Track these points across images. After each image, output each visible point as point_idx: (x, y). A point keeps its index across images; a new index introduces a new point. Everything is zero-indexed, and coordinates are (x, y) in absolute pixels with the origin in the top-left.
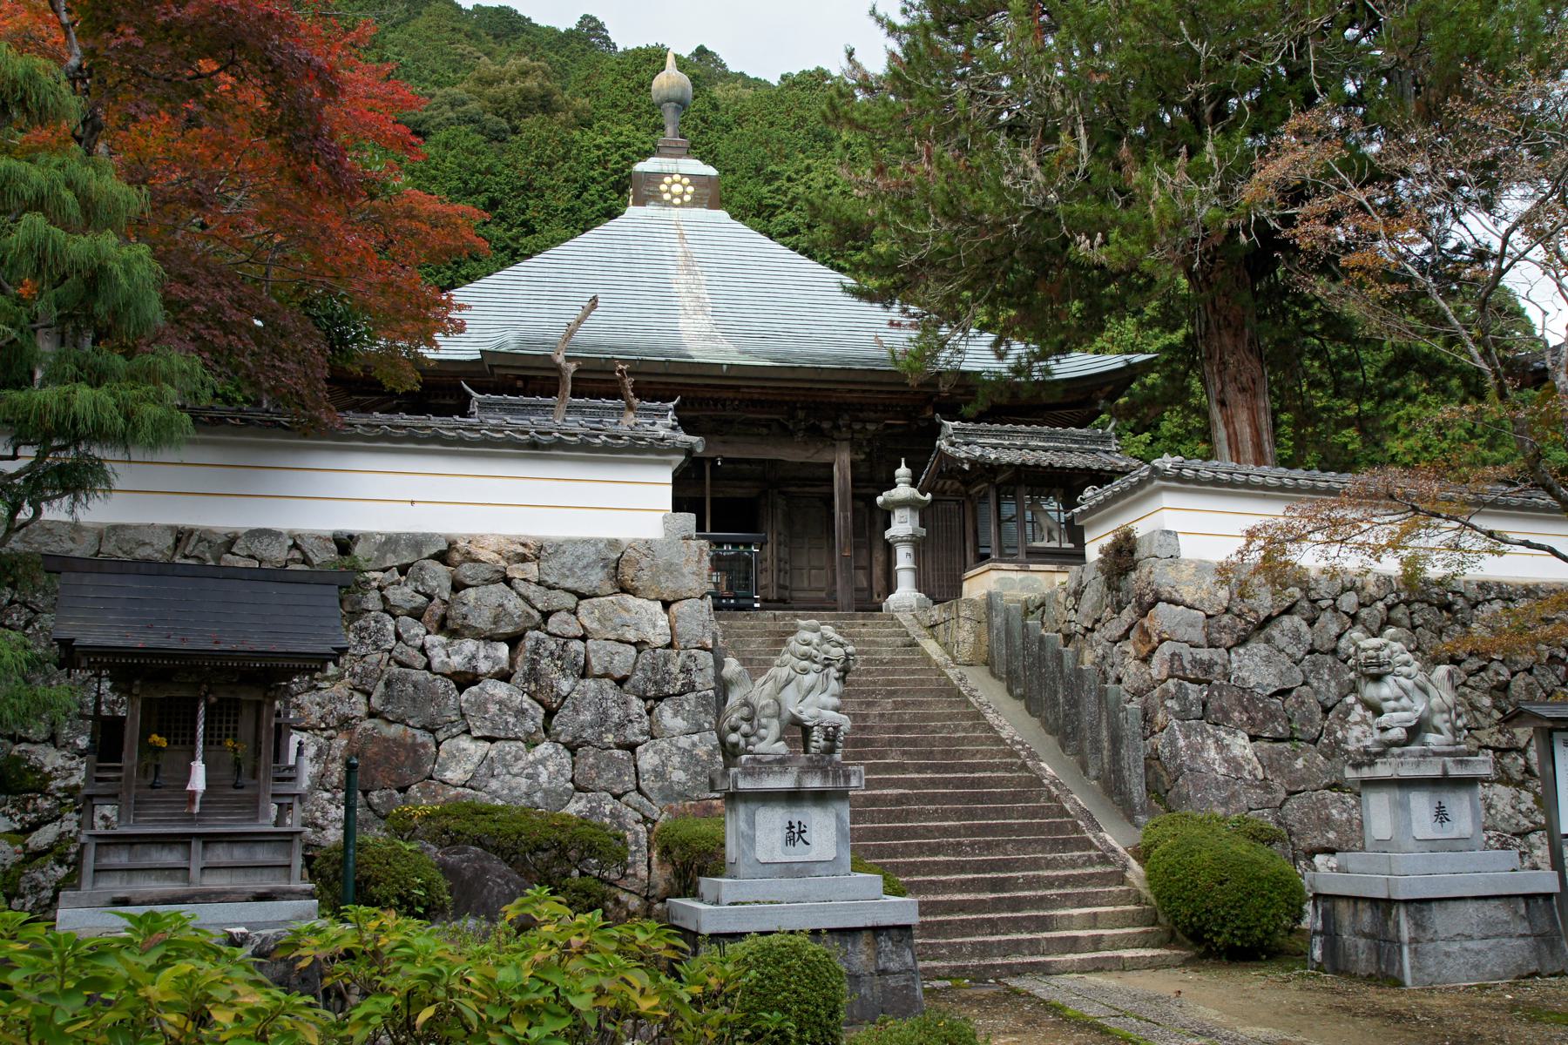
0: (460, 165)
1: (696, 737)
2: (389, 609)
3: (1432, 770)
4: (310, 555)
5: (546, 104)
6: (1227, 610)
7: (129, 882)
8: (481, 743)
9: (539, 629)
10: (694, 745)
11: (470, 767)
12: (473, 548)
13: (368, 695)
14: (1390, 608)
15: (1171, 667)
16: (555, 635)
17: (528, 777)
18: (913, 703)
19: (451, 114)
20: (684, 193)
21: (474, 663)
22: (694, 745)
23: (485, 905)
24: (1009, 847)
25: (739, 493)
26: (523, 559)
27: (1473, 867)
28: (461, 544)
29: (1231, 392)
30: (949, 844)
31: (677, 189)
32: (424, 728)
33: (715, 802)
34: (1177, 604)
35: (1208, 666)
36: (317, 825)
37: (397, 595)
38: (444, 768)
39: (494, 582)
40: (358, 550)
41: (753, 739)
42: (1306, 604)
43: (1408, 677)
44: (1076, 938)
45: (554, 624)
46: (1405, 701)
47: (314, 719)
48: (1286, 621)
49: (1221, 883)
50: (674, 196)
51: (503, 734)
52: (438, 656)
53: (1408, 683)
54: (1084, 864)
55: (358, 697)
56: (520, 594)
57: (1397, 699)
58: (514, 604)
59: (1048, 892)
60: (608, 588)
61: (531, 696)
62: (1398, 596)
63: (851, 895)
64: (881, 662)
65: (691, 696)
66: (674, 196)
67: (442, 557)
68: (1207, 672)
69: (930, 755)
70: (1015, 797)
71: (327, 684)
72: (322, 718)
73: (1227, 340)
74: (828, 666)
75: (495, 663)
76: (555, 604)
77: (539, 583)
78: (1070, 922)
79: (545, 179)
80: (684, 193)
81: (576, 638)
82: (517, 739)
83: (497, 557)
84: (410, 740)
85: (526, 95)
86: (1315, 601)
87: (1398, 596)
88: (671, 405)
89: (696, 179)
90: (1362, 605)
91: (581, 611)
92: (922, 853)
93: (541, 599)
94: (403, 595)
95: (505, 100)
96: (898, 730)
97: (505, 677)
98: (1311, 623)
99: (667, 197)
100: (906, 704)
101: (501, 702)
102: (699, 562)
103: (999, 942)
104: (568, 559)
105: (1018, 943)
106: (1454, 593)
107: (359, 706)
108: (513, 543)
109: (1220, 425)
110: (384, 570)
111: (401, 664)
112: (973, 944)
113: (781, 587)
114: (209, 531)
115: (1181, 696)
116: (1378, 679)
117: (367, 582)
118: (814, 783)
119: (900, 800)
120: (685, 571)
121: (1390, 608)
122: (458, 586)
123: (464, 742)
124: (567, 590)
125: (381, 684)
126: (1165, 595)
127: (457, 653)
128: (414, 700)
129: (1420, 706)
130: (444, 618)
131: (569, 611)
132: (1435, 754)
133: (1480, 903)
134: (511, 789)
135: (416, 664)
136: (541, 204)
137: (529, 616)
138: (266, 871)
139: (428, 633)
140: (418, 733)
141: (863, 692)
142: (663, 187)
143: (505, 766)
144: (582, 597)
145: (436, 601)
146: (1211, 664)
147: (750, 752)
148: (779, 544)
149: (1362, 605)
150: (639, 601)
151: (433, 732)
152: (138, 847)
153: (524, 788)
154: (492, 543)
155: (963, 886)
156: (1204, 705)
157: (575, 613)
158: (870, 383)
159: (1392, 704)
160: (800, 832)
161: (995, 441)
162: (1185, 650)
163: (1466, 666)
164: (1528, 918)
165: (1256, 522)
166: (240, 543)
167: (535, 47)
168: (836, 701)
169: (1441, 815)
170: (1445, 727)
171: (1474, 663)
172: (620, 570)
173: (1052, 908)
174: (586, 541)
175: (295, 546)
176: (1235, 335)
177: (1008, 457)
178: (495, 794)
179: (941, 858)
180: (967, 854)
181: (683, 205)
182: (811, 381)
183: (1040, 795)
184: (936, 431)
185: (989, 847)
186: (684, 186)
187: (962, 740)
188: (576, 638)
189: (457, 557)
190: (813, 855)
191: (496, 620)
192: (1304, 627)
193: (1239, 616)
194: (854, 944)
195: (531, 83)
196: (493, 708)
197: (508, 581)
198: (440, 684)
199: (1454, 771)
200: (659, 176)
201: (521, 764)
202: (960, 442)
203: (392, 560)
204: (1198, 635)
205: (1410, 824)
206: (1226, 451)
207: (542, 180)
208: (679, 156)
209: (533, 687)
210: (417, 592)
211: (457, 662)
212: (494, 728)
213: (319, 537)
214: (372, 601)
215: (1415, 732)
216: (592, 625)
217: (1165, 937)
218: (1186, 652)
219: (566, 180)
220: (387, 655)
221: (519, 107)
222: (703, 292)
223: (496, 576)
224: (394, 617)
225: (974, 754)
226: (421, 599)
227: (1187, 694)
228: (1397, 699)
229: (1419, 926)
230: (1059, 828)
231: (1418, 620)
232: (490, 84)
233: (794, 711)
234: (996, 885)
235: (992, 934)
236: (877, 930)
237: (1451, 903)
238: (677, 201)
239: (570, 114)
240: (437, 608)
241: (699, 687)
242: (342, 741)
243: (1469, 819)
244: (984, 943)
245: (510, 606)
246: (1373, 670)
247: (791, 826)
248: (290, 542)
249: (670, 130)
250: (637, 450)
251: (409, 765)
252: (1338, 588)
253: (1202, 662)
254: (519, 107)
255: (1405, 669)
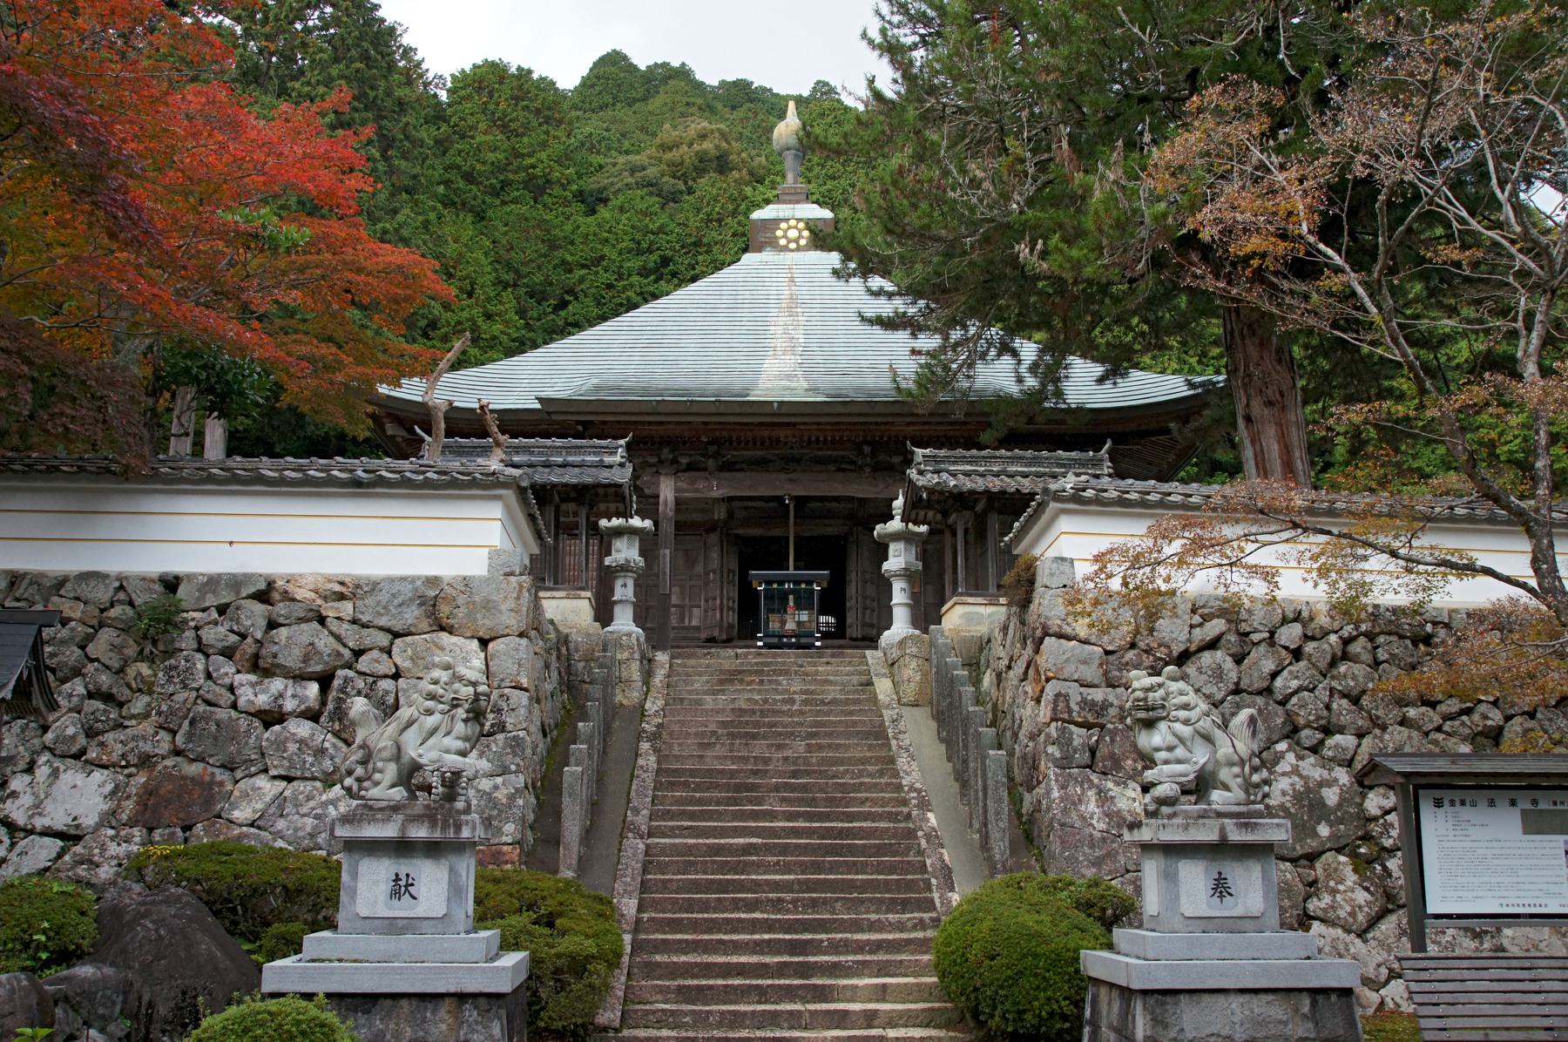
0: (633, 227)
1: (499, 780)
2: (201, 648)
3: (1206, 833)
4: (134, 596)
5: (722, 164)
6: (1133, 646)
8: (277, 783)
9: (350, 668)
10: (496, 787)
11: (260, 806)
12: (290, 588)
14: (1346, 642)
15: (1054, 709)
16: (364, 674)
17: (317, 817)
18: (830, 746)
19: (630, 180)
20: (800, 237)
21: (280, 701)
22: (496, 787)
23: (123, 951)
24: (838, 905)
25: (829, 531)
26: (341, 597)
27: (1217, 954)
28: (280, 583)
29: (1257, 408)
30: (769, 900)
31: (793, 234)
32: (223, 766)
33: (505, 848)
34: (1068, 638)
35: (1101, 708)
37: (209, 635)
38: (234, 807)
39: (308, 621)
40: (182, 591)
41: (366, 784)
42: (1233, 638)
43: (1186, 722)
44: (846, 1013)
45: (364, 664)
46: (1180, 752)
47: (115, 757)
48: (1207, 658)
49: (992, 958)
50: (790, 241)
51: (299, 774)
52: (246, 696)
53: (1185, 731)
54: (914, 928)
55: (162, 733)
56: (332, 633)
57: (1170, 749)
58: (325, 642)
59: (842, 958)
60: (424, 625)
61: (336, 734)
62: (1357, 628)
63: (448, 957)
64: (823, 702)
65: (500, 737)
66: (790, 241)
67: (263, 596)
68: (1099, 715)
69: (812, 802)
70: (880, 850)
71: (134, 722)
72: (123, 756)
73: (1253, 351)
74: (456, 706)
75: (302, 702)
76: (367, 642)
77: (354, 622)
78: (853, 994)
79: (714, 234)
80: (800, 237)
81: (386, 676)
82: (314, 779)
83: (313, 595)
84: (207, 778)
85: (702, 158)
86: (1247, 634)
87: (1357, 628)
88: (622, 442)
89: (812, 226)
90: (1307, 638)
91: (395, 650)
92: (737, 909)
93: (353, 637)
94: (217, 634)
95: (682, 163)
96: (794, 775)
97: (313, 716)
98: (1239, 660)
99: (783, 242)
100: (820, 747)
101: (302, 742)
102: (518, 598)
103: (753, 1012)
104: (383, 597)
105: (776, 1014)
106: (1435, 624)
107: (164, 743)
108: (330, 581)
109: (1247, 443)
110: (204, 610)
111: (209, 703)
112: (722, 1013)
113: (864, 625)
114: (43, 575)
115: (1064, 741)
116: (1149, 724)
117: (185, 621)
118: (420, 832)
119: (748, 849)
120: (503, 608)
121: (1346, 642)
122: (272, 625)
123: (262, 782)
124: (381, 629)
125: (187, 722)
126: (1055, 629)
127: (263, 691)
128: (215, 738)
129: (1201, 756)
130: (256, 656)
131: (382, 650)
132: (1219, 815)
133: (1247, 997)
134: (296, 830)
135: (222, 703)
136: (709, 258)
137: (339, 654)
139: (239, 672)
140: (217, 771)
141: (780, 734)
142: (779, 233)
143: (296, 806)
144: (397, 635)
145: (249, 640)
146: (1106, 705)
147: (362, 798)
148: (865, 582)
149: (1307, 638)
150: (454, 639)
151: (232, 770)
153: (308, 829)
154: (309, 582)
155: (757, 948)
156: (1093, 752)
157: (389, 653)
158: (892, 415)
159: (1162, 755)
160: (407, 886)
161: (968, 468)
162: (1074, 692)
163: (1442, 708)
164: (1314, 1016)
165: (1103, 545)
166: (69, 585)
167: (756, 114)
168: (460, 744)
169: (1221, 888)
170: (1235, 783)
171: (1453, 706)
172: (436, 607)
173: (846, 976)
174: (403, 579)
175: (121, 587)
176: (1261, 345)
177: (979, 484)
178: (279, 835)
179: (757, 915)
180: (788, 911)
181: (798, 249)
182: (867, 415)
183: (908, 849)
184: (908, 461)
185: (814, 904)
186: (800, 231)
187: (857, 788)
188: (386, 676)
189: (276, 596)
190: (420, 910)
191: (306, 659)
192: (1229, 664)
193: (1146, 651)
194: (434, 1012)
195: (707, 145)
196: (292, 747)
197: (322, 620)
198: (243, 723)
199: (1236, 836)
200: (776, 222)
201: (312, 804)
202: (930, 470)
203: (211, 600)
204: (1091, 673)
205: (1177, 898)
206: (1254, 471)
207: (712, 235)
208: (798, 202)
209: (337, 726)
210: (232, 631)
211: (262, 700)
212: (290, 768)
213: (144, 579)
214: (187, 640)
215: (1200, 786)
216: (404, 664)
217: (955, 1016)
218: (1074, 692)
219: (734, 235)
220: (194, 694)
221: (696, 168)
222: (799, 335)
223: (310, 615)
224: (207, 656)
225: (863, 802)
226: (234, 638)
227: (1071, 740)
228: (1170, 749)
229: (1157, 1021)
230: (910, 886)
231: (1382, 655)
232: (670, 149)
233: (413, 755)
234: (794, 948)
235: (759, 1002)
236: (462, 997)
237: (1206, 998)
238: (793, 246)
239: (744, 171)
240: (249, 647)
241: (509, 727)
243: (1260, 893)
244: (735, 1013)
245: (320, 644)
246: (1142, 715)
247: (397, 878)
248: (117, 584)
249: (790, 177)
250: (486, 485)
251: (202, 801)
252: (1278, 618)
253: (1093, 703)
254: (696, 168)
255: (1182, 714)
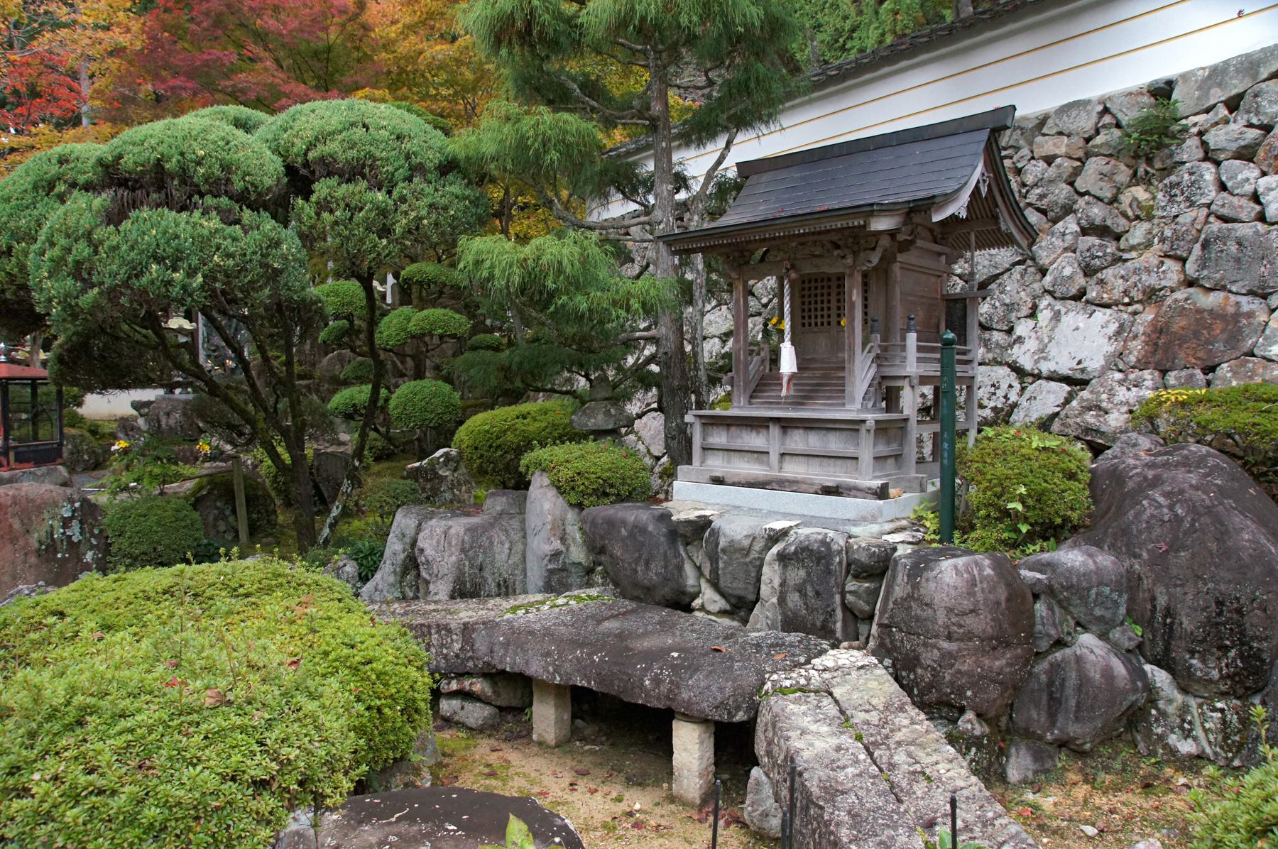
2: (1209, 155)
7: (729, 462)
13: (1184, 261)
32: (1251, 293)
36: (1100, 408)
47: (1116, 295)
55: (1169, 263)
71: (1134, 254)
72: (1126, 293)
84: (1231, 310)
110: (1207, 111)
111: (1225, 219)
117: (1185, 130)
125: (1197, 247)
128: (1238, 260)
135: (1243, 216)
138: (839, 462)
139: (1264, 174)
140: (1244, 300)
151: (1265, 297)
152: (733, 429)
166: (1050, 122)
175: (1106, 110)
210: (1251, 126)
213: (1130, 94)
220: (1204, 211)
224: (1218, 164)
226: (1254, 134)
242: (1148, 316)
248: (1100, 108)
